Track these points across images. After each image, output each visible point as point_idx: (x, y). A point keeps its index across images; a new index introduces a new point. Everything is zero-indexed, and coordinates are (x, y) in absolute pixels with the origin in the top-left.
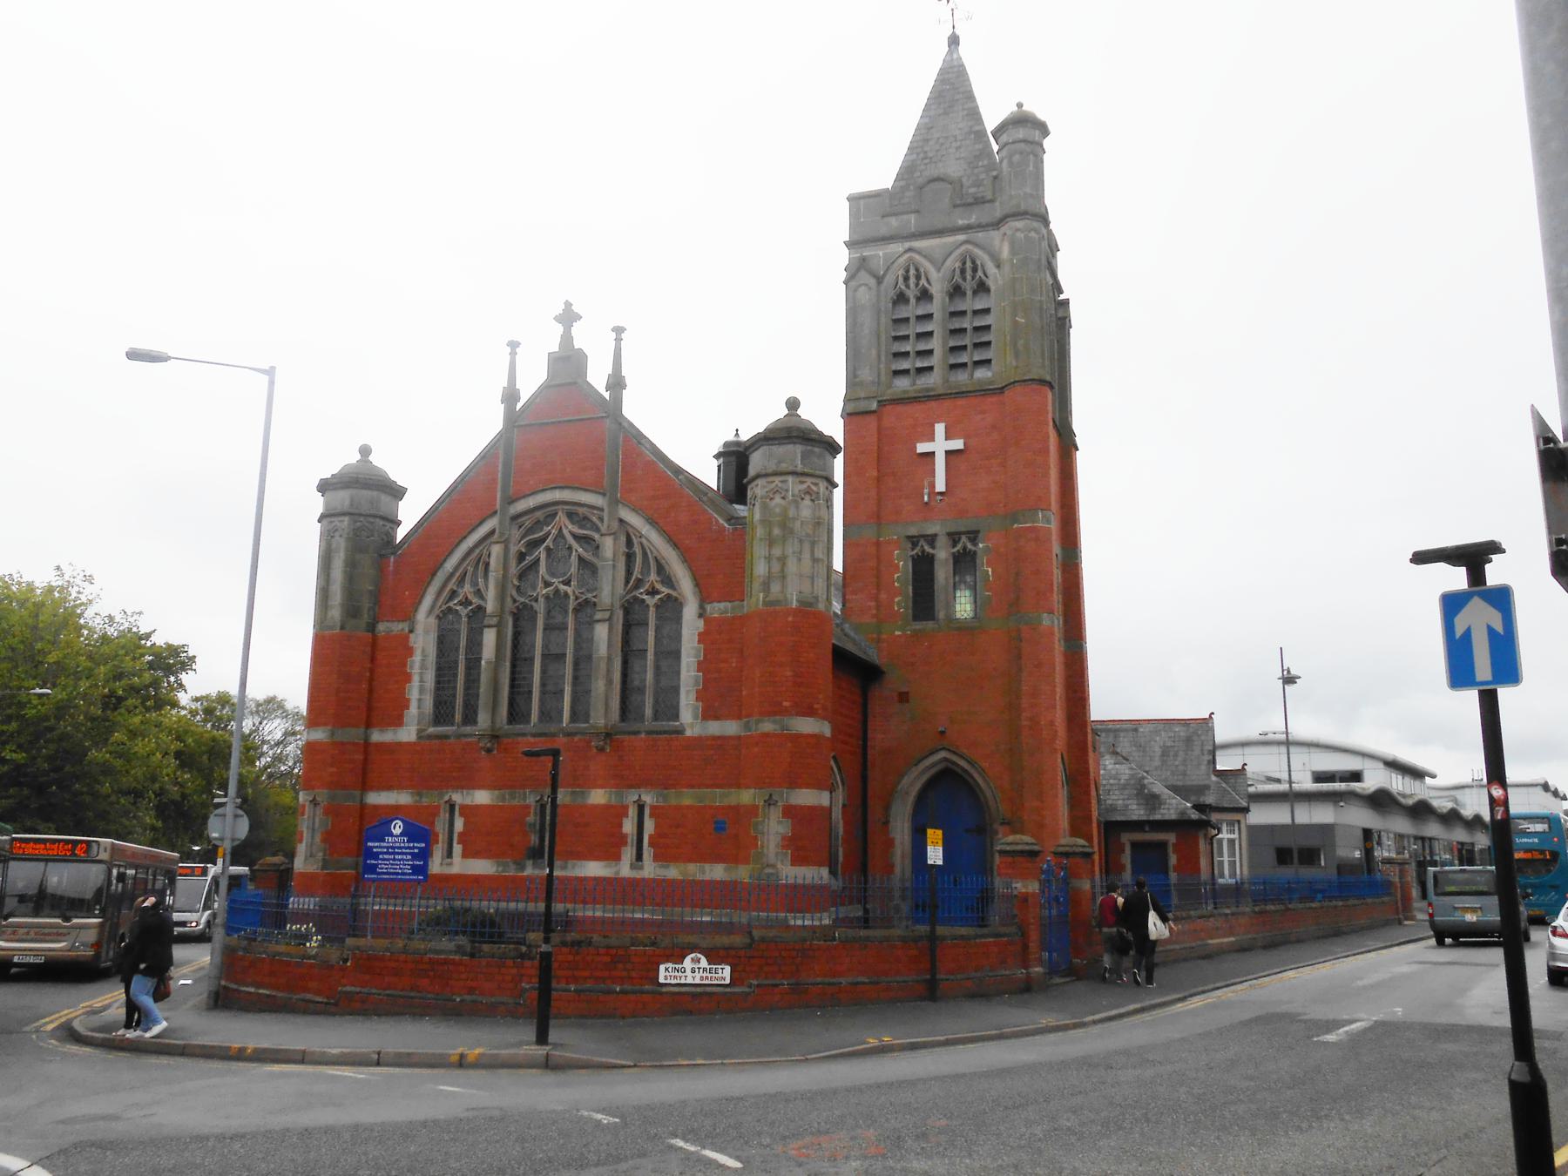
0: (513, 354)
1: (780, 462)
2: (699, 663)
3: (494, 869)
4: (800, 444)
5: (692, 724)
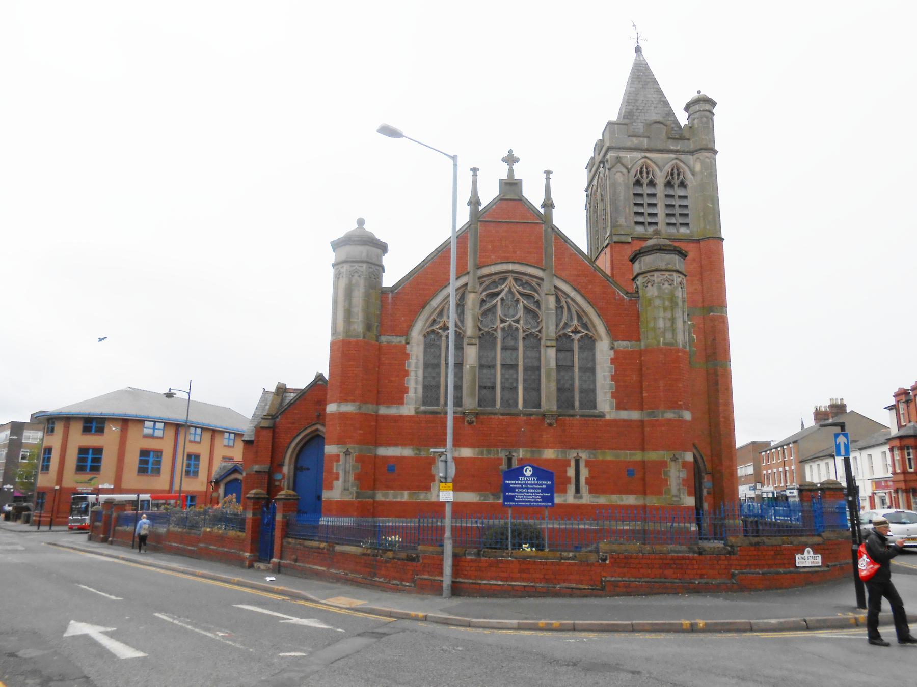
0: (475, 175)
1: (668, 264)
2: (612, 376)
3: (478, 498)
4: (678, 255)
5: (610, 411)
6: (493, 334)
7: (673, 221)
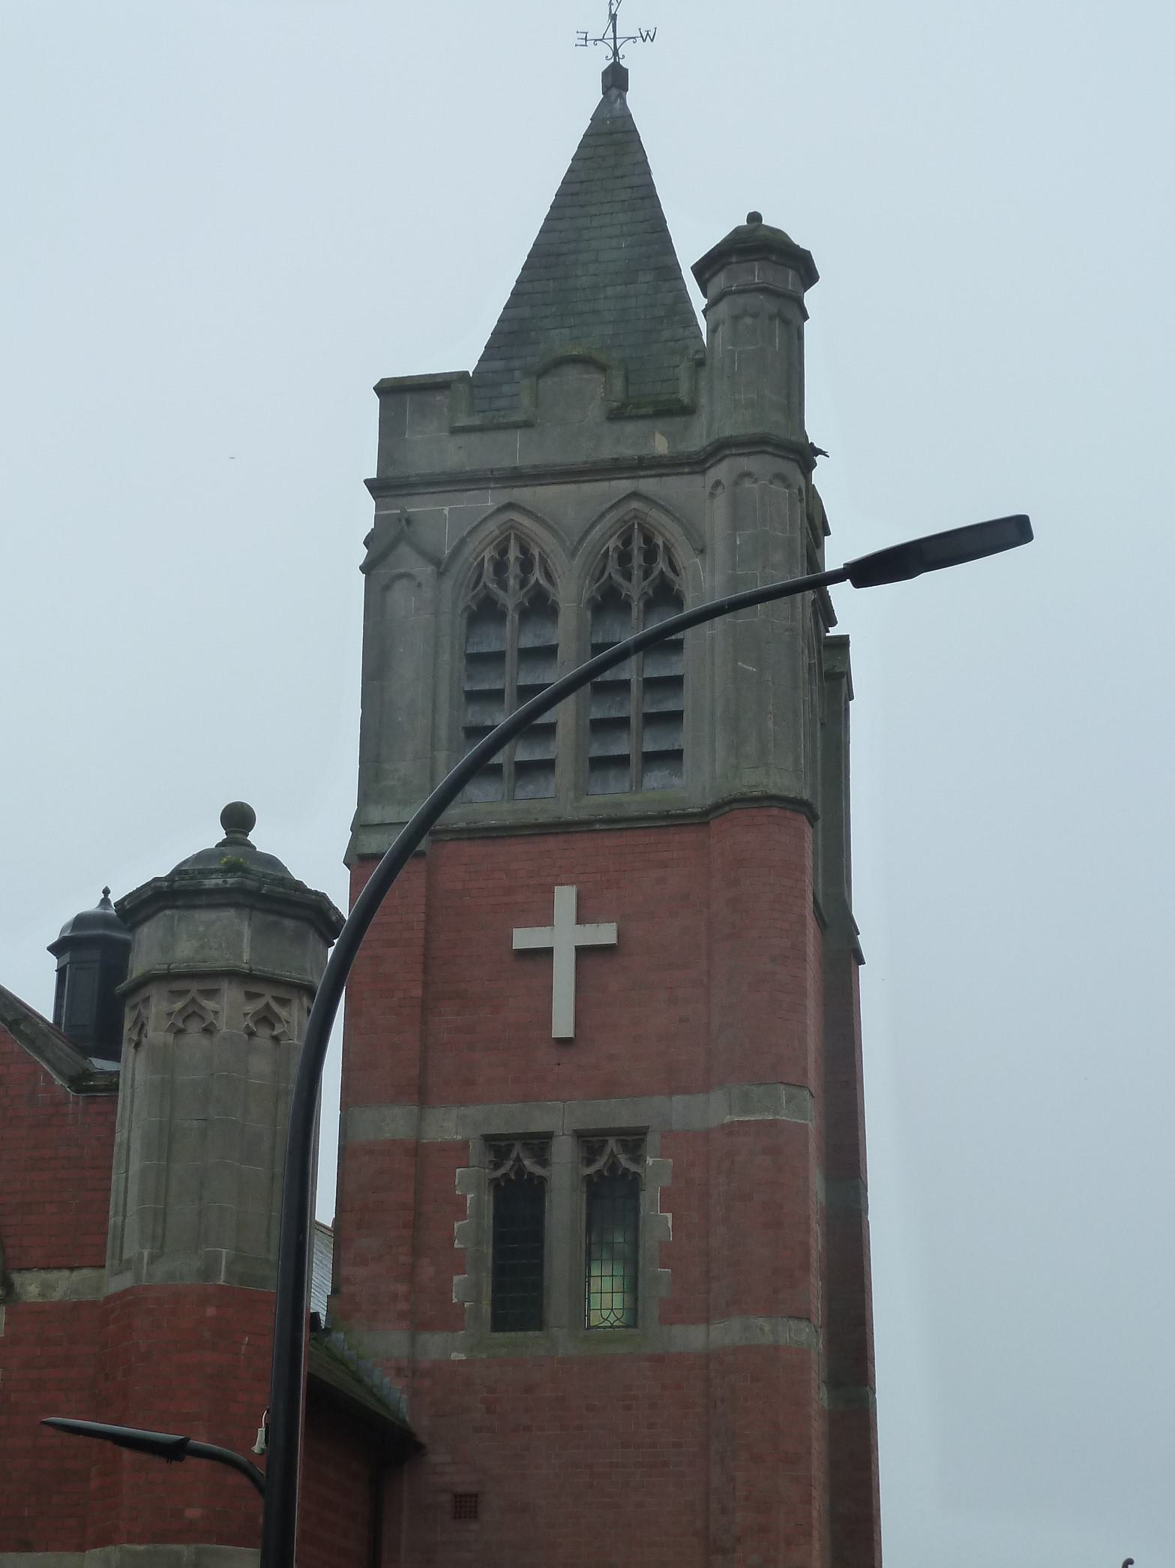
7: (620, 747)
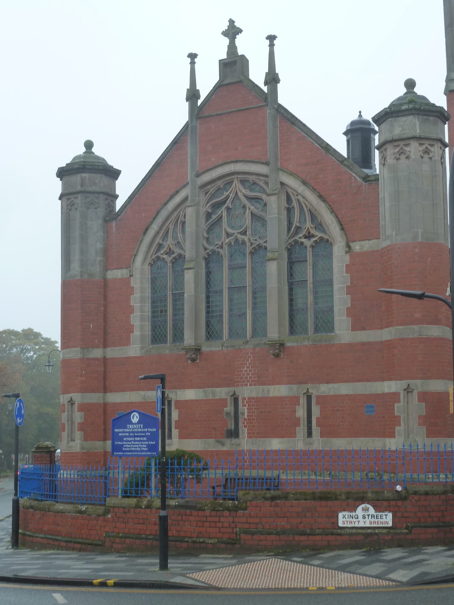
6: (218, 253)
